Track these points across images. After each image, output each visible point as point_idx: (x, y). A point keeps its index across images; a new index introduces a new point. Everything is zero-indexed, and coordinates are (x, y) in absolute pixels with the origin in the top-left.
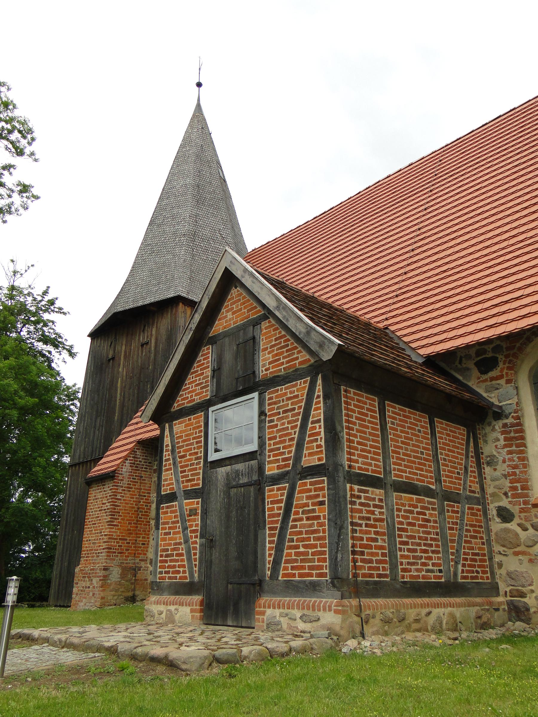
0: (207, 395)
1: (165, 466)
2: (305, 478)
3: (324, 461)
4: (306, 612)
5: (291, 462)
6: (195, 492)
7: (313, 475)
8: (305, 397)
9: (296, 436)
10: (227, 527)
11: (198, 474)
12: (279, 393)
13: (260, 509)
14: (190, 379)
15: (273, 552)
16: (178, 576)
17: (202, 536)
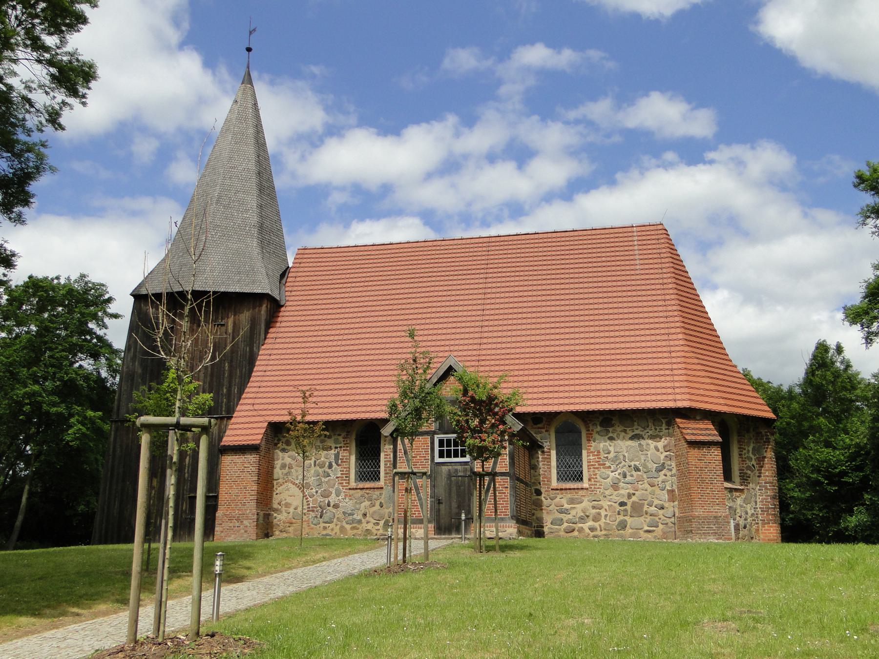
10: (450, 494)
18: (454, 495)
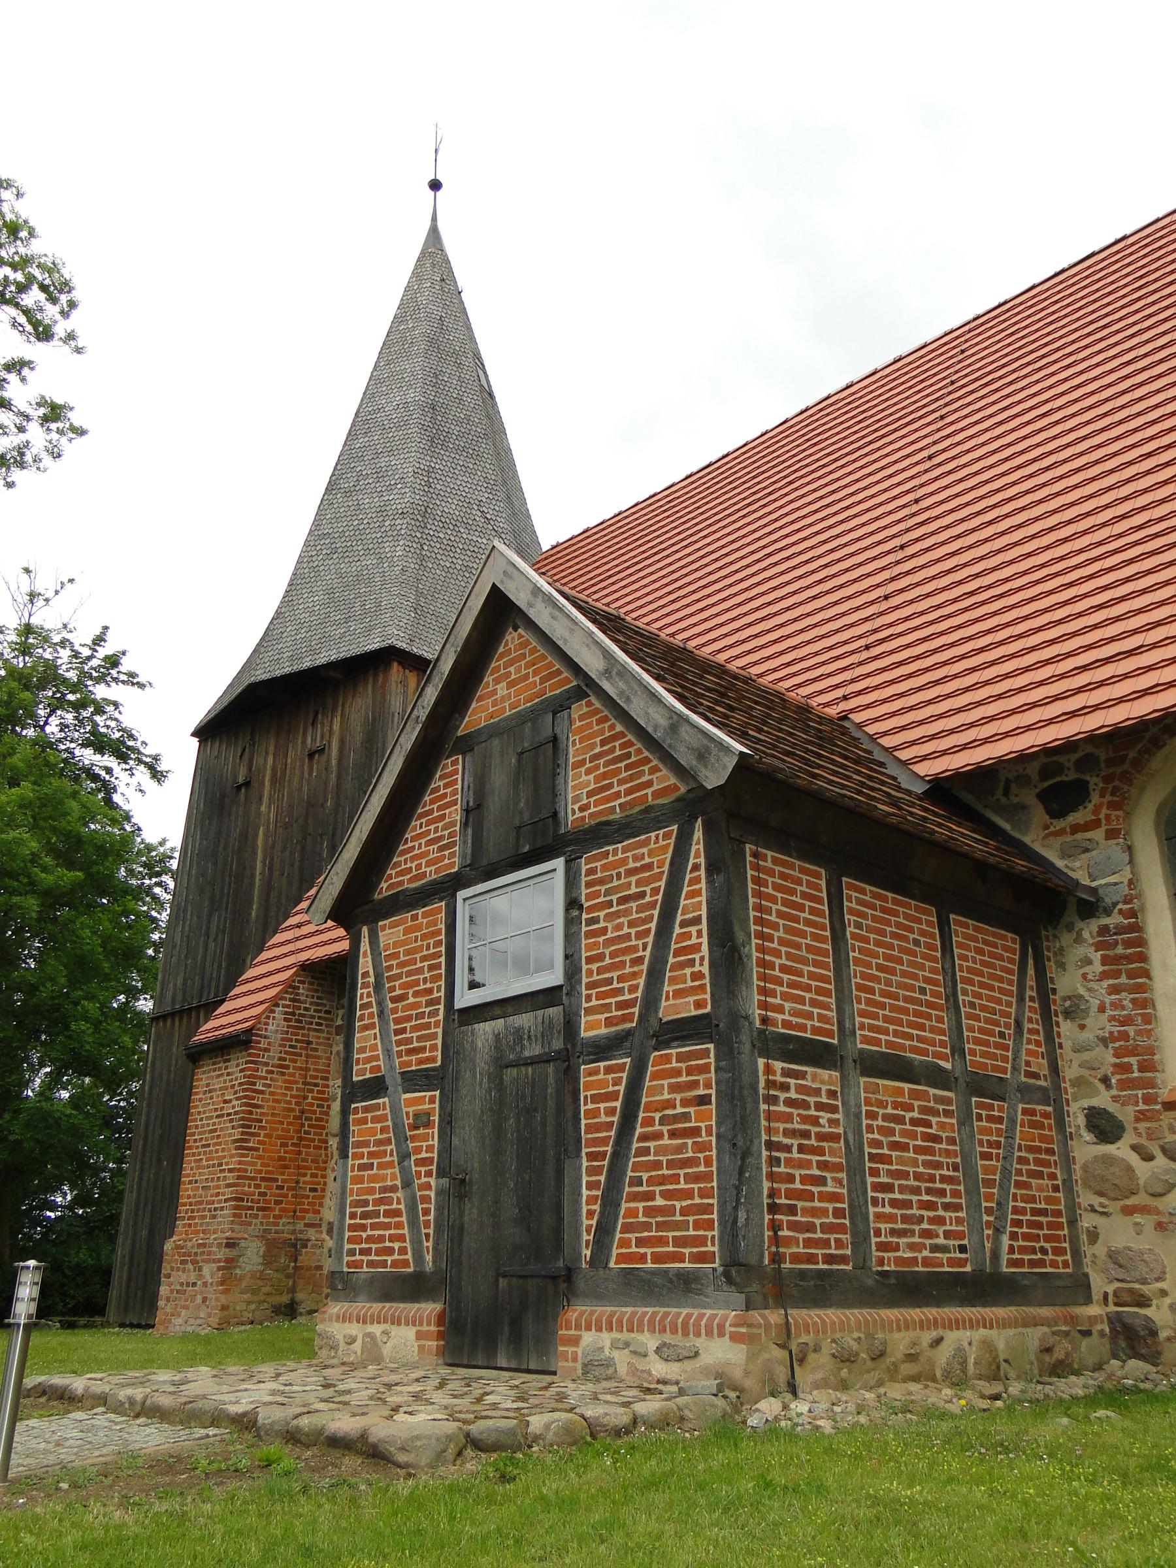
0: (453, 863)
1: (362, 1018)
2: (667, 1044)
3: (708, 1009)
4: (668, 1338)
5: (636, 1010)
6: (427, 1077)
7: (683, 1039)
8: (666, 868)
9: (648, 953)
10: (497, 1153)
11: (434, 1036)
12: (611, 858)
13: (569, 1114)
14: (415, 829)
15: (596, 1207)
16: (389, 1259)
17: (441, 1173)
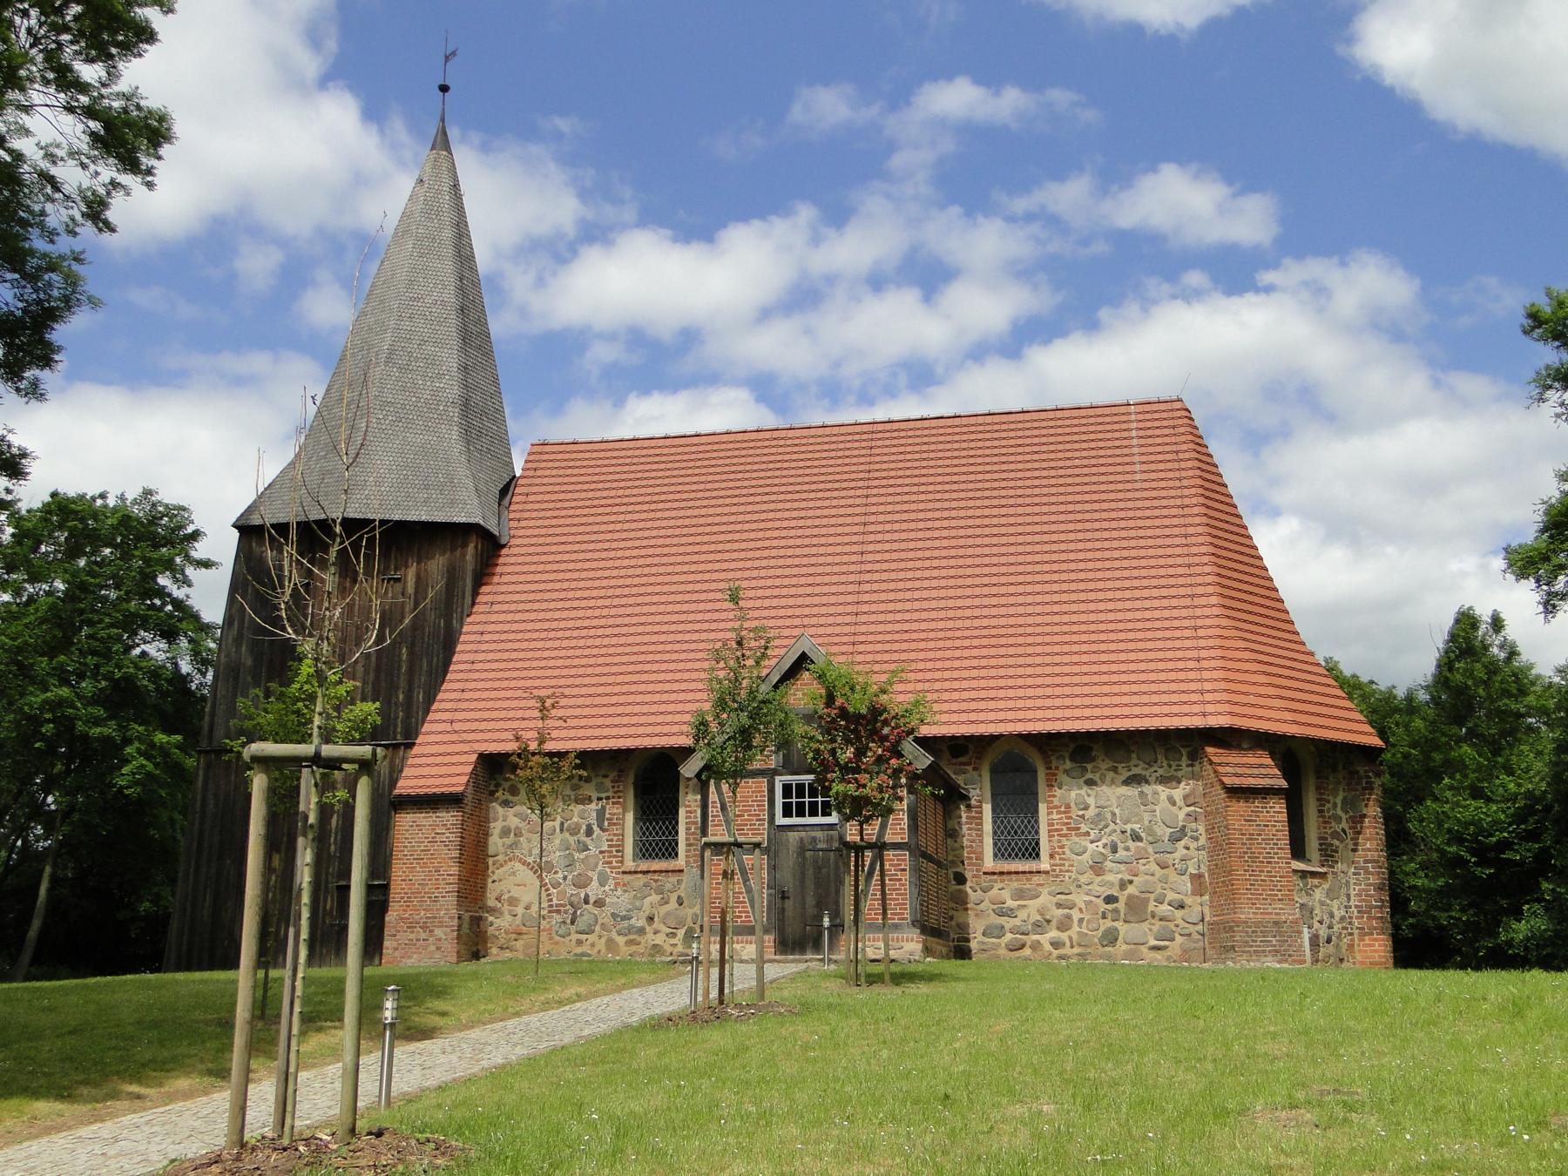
10: (802, 881)
18: (810, 884)
